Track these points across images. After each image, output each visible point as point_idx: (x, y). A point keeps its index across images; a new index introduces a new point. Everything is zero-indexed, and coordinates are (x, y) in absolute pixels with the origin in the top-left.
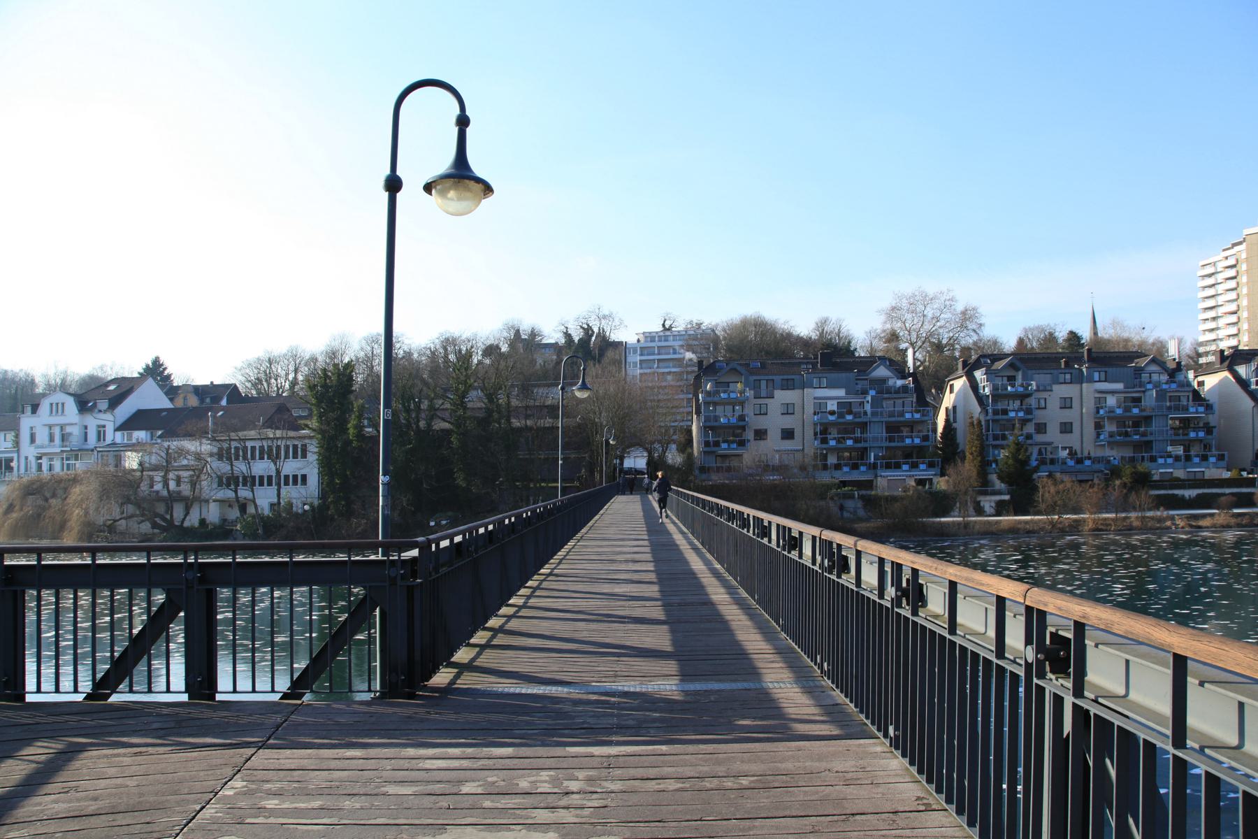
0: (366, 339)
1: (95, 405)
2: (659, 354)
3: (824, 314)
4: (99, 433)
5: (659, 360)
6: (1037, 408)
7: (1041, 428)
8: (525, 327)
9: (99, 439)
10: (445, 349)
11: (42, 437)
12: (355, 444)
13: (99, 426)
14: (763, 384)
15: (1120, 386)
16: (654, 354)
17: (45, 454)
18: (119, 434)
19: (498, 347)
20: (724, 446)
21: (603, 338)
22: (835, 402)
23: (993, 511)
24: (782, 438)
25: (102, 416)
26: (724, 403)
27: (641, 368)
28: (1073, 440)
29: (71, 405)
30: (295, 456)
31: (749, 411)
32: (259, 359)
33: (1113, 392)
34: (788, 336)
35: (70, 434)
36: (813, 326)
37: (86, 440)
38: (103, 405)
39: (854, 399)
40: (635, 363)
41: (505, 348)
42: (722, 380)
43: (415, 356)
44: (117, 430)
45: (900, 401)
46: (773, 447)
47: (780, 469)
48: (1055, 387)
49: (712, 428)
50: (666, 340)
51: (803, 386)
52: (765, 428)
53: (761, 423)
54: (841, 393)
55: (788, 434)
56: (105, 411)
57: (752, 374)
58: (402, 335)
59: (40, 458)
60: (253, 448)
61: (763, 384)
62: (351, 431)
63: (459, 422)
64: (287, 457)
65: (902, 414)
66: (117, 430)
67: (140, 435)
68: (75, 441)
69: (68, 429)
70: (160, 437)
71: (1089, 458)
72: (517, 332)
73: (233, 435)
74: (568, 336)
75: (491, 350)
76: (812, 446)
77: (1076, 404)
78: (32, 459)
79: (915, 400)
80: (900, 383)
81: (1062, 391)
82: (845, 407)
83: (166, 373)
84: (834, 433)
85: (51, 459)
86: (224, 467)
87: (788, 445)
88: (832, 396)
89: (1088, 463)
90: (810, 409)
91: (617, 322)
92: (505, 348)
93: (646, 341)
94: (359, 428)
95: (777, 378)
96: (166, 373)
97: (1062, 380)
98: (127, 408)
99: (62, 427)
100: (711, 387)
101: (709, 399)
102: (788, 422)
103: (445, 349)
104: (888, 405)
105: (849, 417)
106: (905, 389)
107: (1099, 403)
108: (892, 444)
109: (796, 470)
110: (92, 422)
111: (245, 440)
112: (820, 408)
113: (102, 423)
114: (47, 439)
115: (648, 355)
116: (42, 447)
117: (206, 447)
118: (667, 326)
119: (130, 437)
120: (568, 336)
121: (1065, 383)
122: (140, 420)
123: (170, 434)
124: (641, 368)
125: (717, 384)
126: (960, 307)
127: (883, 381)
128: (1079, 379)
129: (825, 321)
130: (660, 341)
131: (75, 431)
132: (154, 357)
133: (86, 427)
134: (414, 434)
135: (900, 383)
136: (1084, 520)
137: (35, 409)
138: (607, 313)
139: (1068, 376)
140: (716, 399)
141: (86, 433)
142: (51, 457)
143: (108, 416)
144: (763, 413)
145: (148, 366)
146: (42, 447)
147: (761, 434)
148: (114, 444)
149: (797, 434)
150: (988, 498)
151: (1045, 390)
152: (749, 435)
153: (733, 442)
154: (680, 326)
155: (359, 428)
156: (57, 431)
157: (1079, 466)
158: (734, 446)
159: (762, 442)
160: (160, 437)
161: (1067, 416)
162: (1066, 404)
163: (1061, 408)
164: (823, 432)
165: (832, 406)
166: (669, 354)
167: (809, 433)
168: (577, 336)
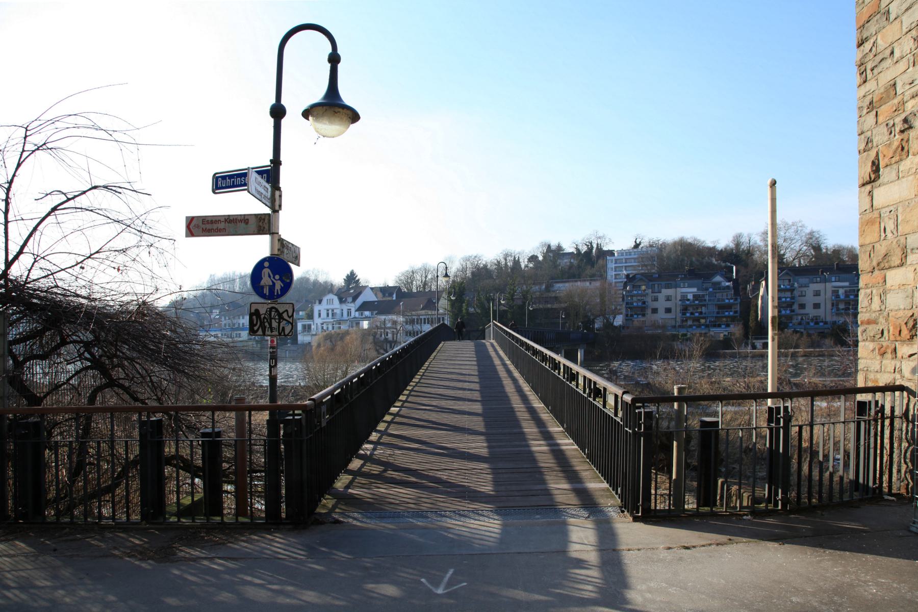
0: (462, 258)
1: (346, 300)
2: (626, 263)
3: (738, 231)
4: (348, 312)
5: (626, 267)
6: (799, 296)
7: (802, 306)
8: (554, 244)
9: (348, 315)
10: (506, 260)
11: (324, 314)
12: (465, 317)
13: (348, 309)
14: (656, 286)
15: (847, 284)
16: (622, 263)
17: (325, 322)
18: (357, 313)
19: (537, 257)
20: (635, 316)
21: (599, 249)
22: (692, 295)
23: (761, 347)
24: (666, 312)
25: (349, 305)
26: (637, 295)
27: (615, 271)
28: (820, 312)
29: (336, 299)
30: (428, 323)
31: (649, 299)
32: (407, 271)
33: (842, 287)
34: (712, 251)
35: (336, 313)
36: (731, 239)
37: (342, 315)
38: (350, 299)
39: (701, 293)
40: (612, 268)
41: (541, 258)
42: (636, 284)
43: (489, 266)
44: (356, 311)
45: (725, 294)
46: (661, 315)
47: (663, 327)
48: (811, 285)
49: (629, 308)
50: (630, 255)
51: (676, 287)
52: (804, 303)
53: (655, 305)
54: (695, 290)
55: (668, 310)
56: (351, 303)
57: (650, 281)
58: (482, 256)
59: (323, 324)
60: (425, 319)
61: (656, 286)
62: (464, 311)
63: (511, 307)
64: (425, 323)
65: (723, 300)
66: (356, 311)
67: (367, 313)
68: (338, 317)
69: (335, 311)
70: (376, 314)
71: (822, 322)
72: (549, 246)
73: (414, 313)
74: (577, 249)
75: (533, 258)
76: (676, 314)
77: (822, 293)
78: (319, 324)
79: (733, 293)
80: (727, 284)
81: (814, 287)
82: (696, 297)
83: (357, 279)
84: (691, 310)
85: (328, 325)
86: (409, 327)
87: (669, 316)
88: (690, 291)
89: (821, 324)
90: (829, 294)
91: (607, 241)
92: (541, 258)
93: (618, 256)
94: (467, 310)
95: (663, 283)
96: (357, 279)
97: (815, 281)
98: (360, 301)
99: (333, 310)
100: (630, 288)
101: (628, 294)
102: (668, 304)
103: (506, 260)
104: (719, 296)
105: (697, 302)
106: (728, 287)
107: (835, 293)
108: (718, 315)
109: (670, 328)
110: (345, 307)
111: (419, 315)
112: (684, 298)
113: (349, 308)
114: (326, 315)
115: (620, 263)
116: (324, 319)
117: (401, 319)
118: (638, 242)
119: (362, 315)
120: (577, 249)
121: (817, 283)
122: (365, 306)
123: (381, 312)
124: (615, 271)
125: (634, 286)
126: (808, 231)
127: (719, 283)
128: (825, 281)
129: (740, 236)
130: (626, 255)
131: (338, 312)
132: (351, 270)
133: (342, 310)
134: (104, 363)
135: (727, 284)
136: (798, 352)
137: (320, 302)
138: (602, 235)
139: (818, 279)
140: (631, 294)
141: (342, 313)
142: (327, 323)
143: (352, 305)
144: (656, 299)
145: (348, 275)
146: (324, 319)
147: (655, 311)
148: (355, 318)
149: (673, 310)
150: (759, 341)
151: (805, 287)
152: (649, 311)
153: (639, 314)
154: (645, 243)
155: (467, 310)
156: (330, 312)
157: (817, 326)
158: (640, 316)
159: (655, 315)
160: (376, 314)
161: (817, 300)
162: (817, 293)
163: (814, 296)
164: (685, 309)
165: (690, 297)
166: (631, 262)
167: (829, 306)
168: (584, 249)
